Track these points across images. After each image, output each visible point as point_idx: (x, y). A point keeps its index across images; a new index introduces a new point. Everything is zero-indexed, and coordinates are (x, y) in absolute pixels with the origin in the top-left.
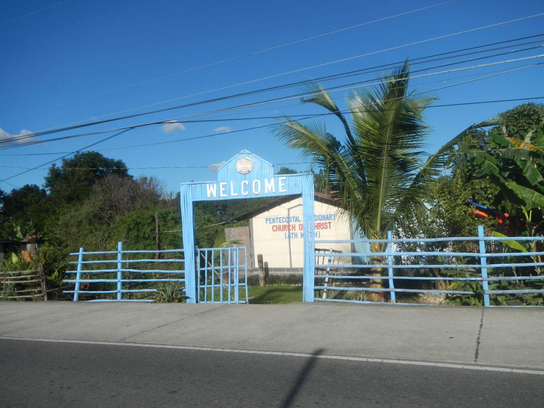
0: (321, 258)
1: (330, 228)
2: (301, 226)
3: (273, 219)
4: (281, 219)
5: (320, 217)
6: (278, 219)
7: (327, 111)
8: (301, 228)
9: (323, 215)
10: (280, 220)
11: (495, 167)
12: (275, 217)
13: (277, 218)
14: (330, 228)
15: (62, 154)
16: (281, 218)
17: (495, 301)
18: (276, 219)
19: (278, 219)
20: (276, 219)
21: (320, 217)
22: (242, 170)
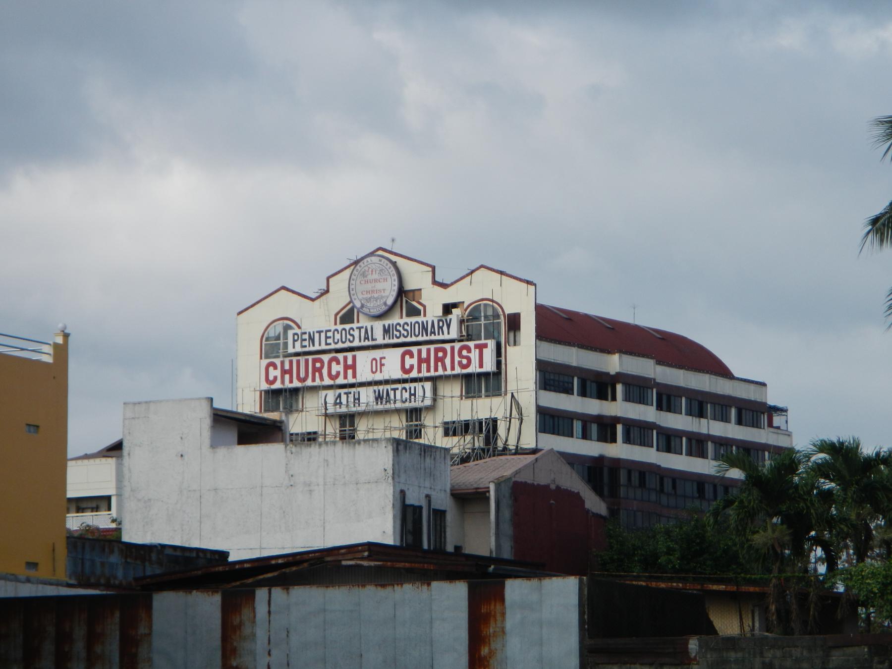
0: (474, 355)
1: (381, 372)
2: (374, 362)
3: (310, 334)
4: (329, 334)
5: (417, 325)
6: (323, 335)
7: (469, 278)
8: (374, 370)
9: (423, 323)
10: (327, 338)
11: (492, 379)
12: (315, 330)
13: (320, 332)
14: (381, 372)
15: (495, 412)
16: (330, 331)
17: (466, 398)
18: (317, 335)
19: (323, 335)
20: (317, 335)
21: (417, 325)
22: (368, 300)
